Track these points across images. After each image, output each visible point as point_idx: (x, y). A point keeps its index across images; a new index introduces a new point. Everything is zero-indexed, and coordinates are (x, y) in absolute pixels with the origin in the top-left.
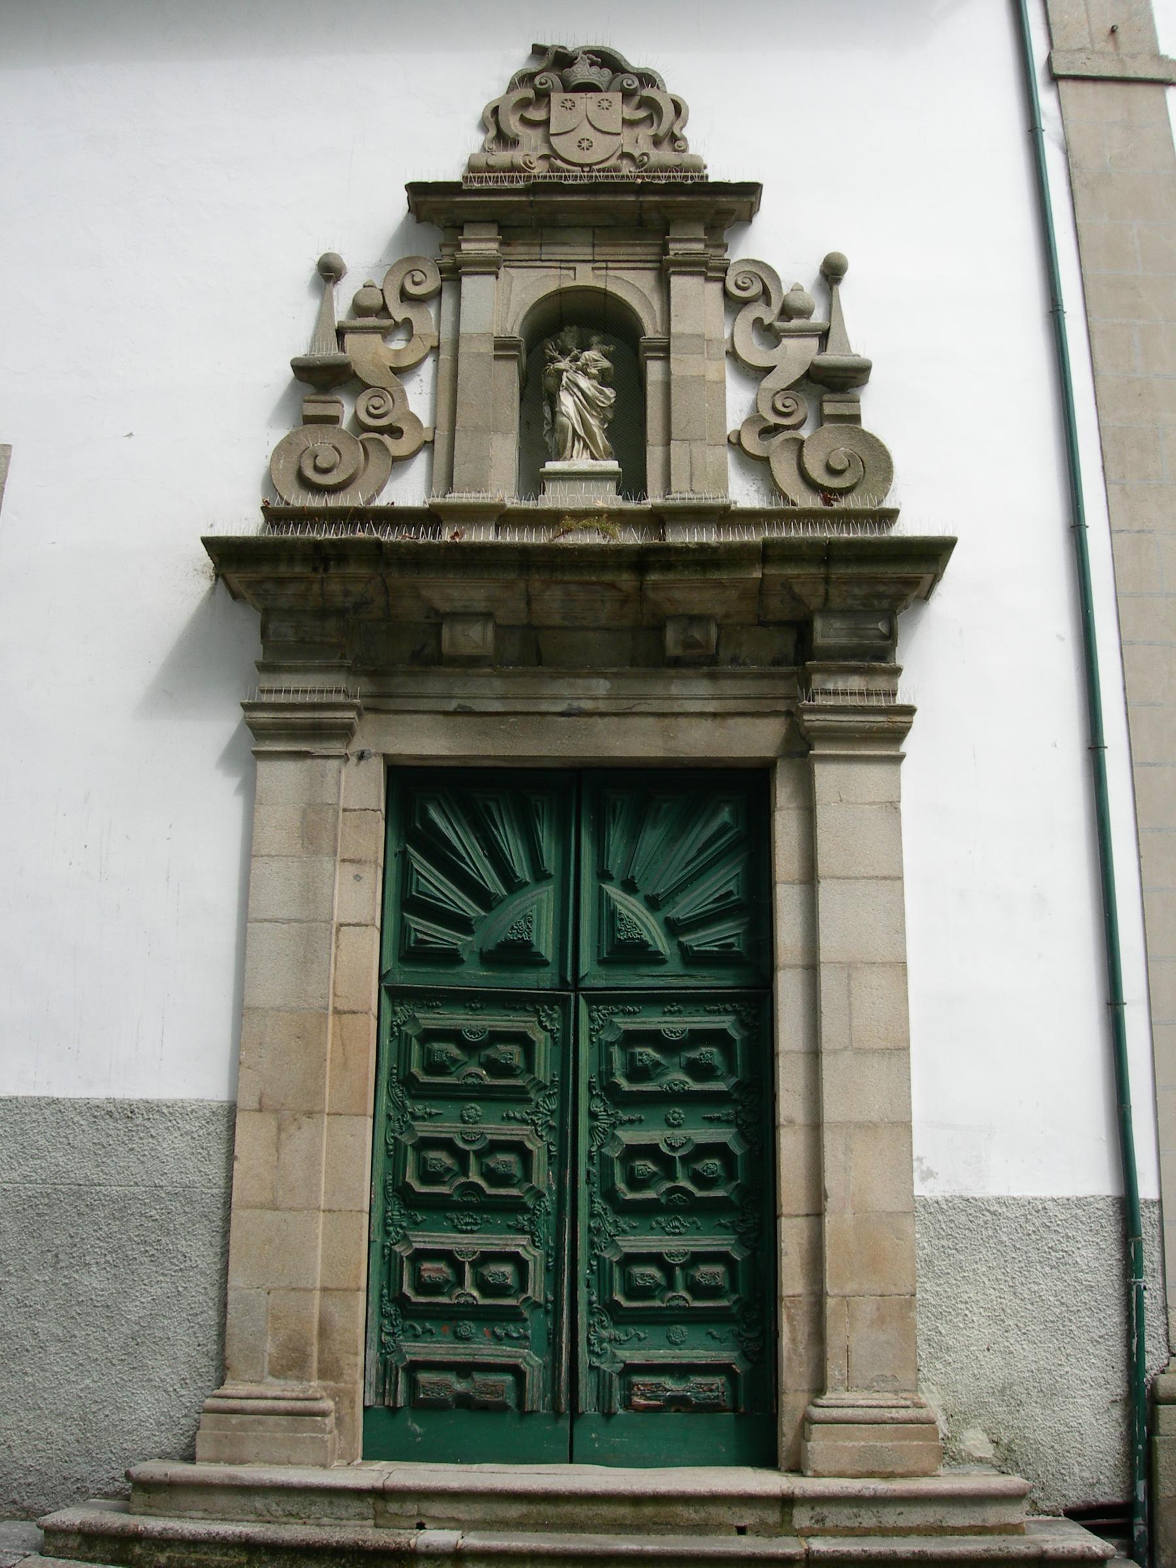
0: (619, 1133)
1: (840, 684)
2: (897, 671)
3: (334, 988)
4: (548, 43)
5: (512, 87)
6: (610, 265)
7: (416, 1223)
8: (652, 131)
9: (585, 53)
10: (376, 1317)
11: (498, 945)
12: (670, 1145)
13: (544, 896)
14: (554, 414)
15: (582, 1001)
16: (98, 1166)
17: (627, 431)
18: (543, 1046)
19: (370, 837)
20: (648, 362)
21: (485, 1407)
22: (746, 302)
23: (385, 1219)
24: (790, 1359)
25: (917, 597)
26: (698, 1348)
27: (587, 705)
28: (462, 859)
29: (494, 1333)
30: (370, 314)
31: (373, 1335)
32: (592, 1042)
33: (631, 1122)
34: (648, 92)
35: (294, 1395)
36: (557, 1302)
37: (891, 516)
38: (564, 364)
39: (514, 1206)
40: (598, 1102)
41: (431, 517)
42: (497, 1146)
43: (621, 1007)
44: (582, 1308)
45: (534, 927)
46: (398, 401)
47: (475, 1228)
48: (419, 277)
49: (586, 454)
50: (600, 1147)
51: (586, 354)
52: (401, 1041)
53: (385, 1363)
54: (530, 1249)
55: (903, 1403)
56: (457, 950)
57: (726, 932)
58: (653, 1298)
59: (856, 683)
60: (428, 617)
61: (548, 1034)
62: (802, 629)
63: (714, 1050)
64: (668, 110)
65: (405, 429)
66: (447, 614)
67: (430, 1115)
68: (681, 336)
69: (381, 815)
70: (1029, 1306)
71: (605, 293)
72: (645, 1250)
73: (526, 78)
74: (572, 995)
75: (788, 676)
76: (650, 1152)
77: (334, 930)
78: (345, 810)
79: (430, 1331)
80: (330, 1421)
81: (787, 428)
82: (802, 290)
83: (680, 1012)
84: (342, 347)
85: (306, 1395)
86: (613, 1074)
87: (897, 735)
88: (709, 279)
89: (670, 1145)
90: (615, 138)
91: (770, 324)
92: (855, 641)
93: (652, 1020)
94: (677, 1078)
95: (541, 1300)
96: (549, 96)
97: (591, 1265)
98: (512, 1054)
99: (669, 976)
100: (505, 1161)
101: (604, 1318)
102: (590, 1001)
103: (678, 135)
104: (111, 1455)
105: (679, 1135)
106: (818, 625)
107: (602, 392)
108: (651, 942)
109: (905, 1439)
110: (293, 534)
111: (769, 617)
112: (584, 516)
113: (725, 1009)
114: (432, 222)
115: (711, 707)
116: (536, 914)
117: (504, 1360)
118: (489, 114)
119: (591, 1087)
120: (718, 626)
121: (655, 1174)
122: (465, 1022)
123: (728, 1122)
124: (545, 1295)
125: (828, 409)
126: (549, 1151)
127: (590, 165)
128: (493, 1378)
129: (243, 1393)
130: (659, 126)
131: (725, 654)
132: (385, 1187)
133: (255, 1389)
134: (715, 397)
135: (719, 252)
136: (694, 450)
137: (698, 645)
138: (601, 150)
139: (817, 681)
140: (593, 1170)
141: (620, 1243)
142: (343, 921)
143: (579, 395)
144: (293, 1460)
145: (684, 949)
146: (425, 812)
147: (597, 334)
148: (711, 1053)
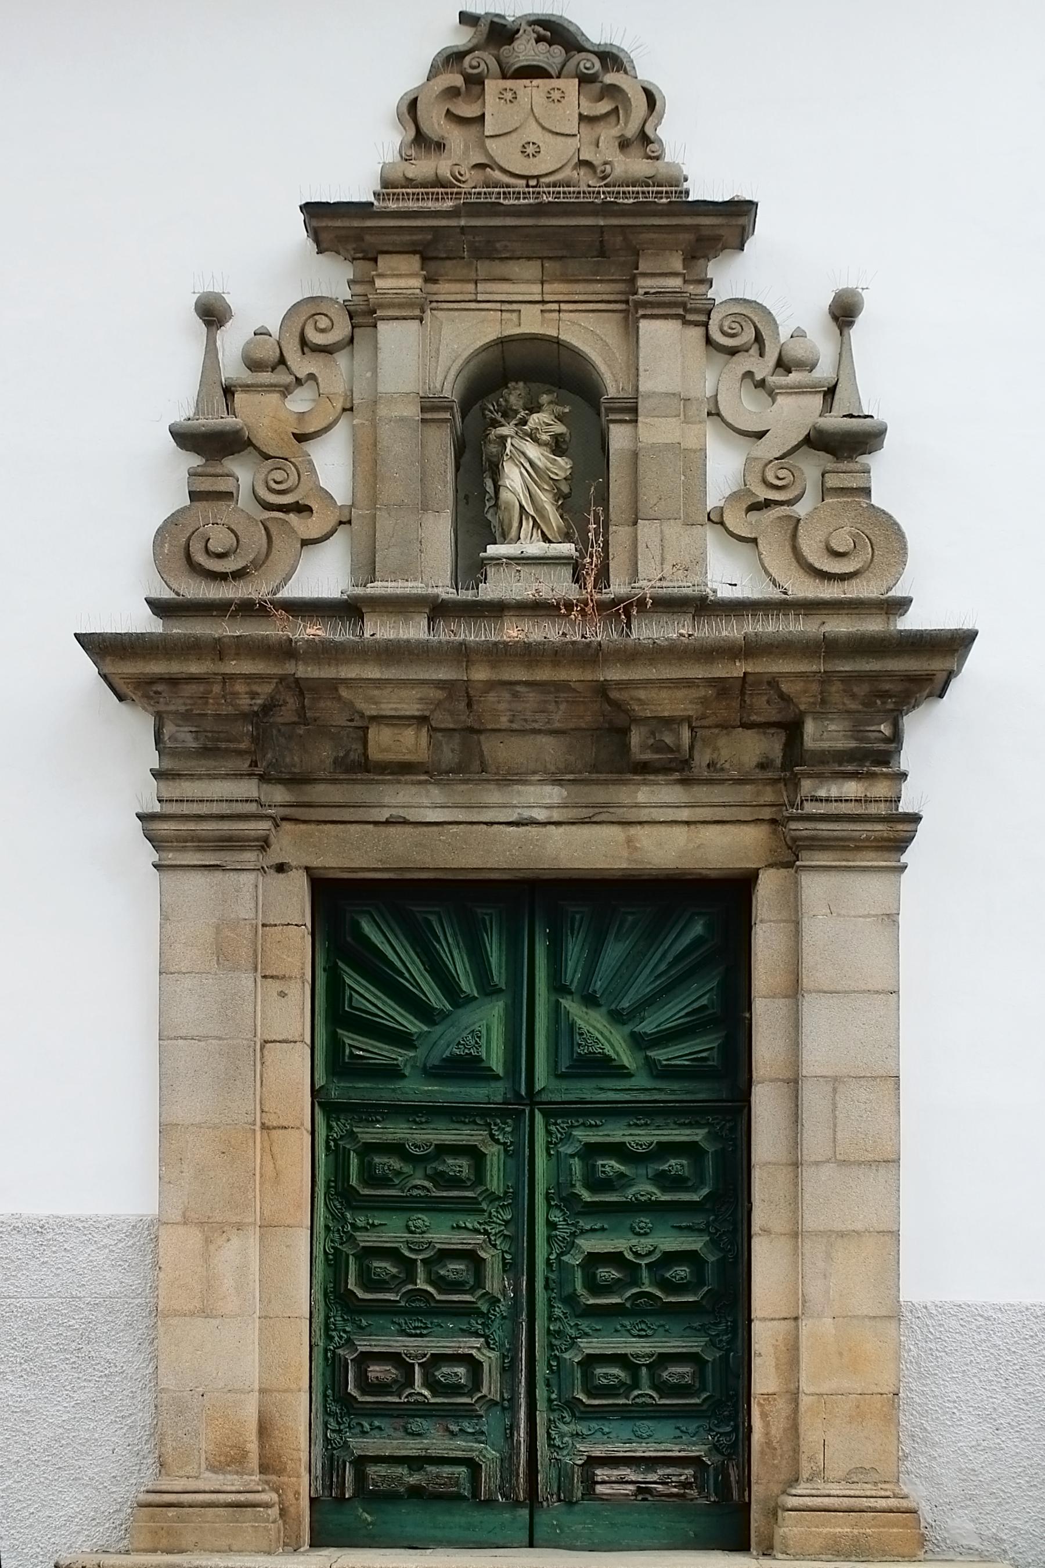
1: (834, 790)
3: (261, 1103)
4: (480, 11)
5: (434, 72)
6: (564, 306)
8: (615, 132)
9: (531, 23)
13: (495, 1012)
14: (497, 489)
15: (539, 1118)
16: (6, 1280)
17: (586, 498)
18: (495, 1158)
19: (296, 950)
20: (611, 426)
21: (439, 1497)
22: (733, 352)
26: (661, 1441)
27: (541, 815)
29: (447, 1430)
30: (267, 364)
31: (318, 1431)
32: (549, 1154)
33: (593, 1230)
34: (610, 78)
35: (234, 1488)
36: (513, 1400)
37: (902, 605)
39: (466, 1311)
40: (558, 1213)
41: (349, 610)
42: (446, 1255)
43: (581, 1121)
44: (541, 1405)
47: (425, 1332)
48: (323, 322)
49: (538, 535)
50: (559, 1255)
51: (535, 416)
52: (337, 1155)
54: (485, 1351)
55: (883, 1493)
56: (398, 1065)
58: (617, 1396)
59: (852, 788)
60: (352, 720)
61: (502, 1147)
62: (793, 729)
63: (684, 1162)
64: (639, 102)
65: (315, 507)
67: (373, 1225)
68: (651, 395)
69: (306, 931)
70: (1023, 1406)
71: (557, 342)
73: (452, 59)
75: (774, 782)
76: (615, 1259)
77: (258, 1047)
78: (263, 925)
79: (379, 1428)
80: (274, 1512)
81: (781, 503)
83: (646, 1124)
84: (230, 410)
85: (247, 1488)
86: (573, 1186)
87: (901, 844)
88: (686, 323)
90: (570, 140)
91: (763, 381)
92: (853, 744)
93: (617, 1133)
94: (645, 1189)
95: (498, 1398)
96: (483, 83)
98: (461, 1166)
99: (639, 1086)
101: (565, 1414)
102: (546, 1114)
103: (652, 137)
104: (38, 1550)
105: (644, 1244)
106: (810, 728)
108: (614, 1056)
109: (884, 1527)
110: (180, 629)
113: (697, 1122)
114: (338, 253)
115: (684, 814)
116: (486, 1028)
117: (459, 1454)
118: (404, 109)
119: (548, 1198)
120: (692, 729)
122: (408, 1136)
123: (700, 1231)
124: (502, 1393)
125: (832, 481)
127: (538, 177)
128: (446, 1470)
130: (626, 124)
133: (192, 1485)
134: (701, 447)
135: (701, 289)
136: (667, 532)
137: (669, 749)
138: (553, 157)
140: (553, 1276)
141: (582, 1345)
144: (235, 1548)
145: (651, 1065)
147: (549, 392)
148: (682, 1166)
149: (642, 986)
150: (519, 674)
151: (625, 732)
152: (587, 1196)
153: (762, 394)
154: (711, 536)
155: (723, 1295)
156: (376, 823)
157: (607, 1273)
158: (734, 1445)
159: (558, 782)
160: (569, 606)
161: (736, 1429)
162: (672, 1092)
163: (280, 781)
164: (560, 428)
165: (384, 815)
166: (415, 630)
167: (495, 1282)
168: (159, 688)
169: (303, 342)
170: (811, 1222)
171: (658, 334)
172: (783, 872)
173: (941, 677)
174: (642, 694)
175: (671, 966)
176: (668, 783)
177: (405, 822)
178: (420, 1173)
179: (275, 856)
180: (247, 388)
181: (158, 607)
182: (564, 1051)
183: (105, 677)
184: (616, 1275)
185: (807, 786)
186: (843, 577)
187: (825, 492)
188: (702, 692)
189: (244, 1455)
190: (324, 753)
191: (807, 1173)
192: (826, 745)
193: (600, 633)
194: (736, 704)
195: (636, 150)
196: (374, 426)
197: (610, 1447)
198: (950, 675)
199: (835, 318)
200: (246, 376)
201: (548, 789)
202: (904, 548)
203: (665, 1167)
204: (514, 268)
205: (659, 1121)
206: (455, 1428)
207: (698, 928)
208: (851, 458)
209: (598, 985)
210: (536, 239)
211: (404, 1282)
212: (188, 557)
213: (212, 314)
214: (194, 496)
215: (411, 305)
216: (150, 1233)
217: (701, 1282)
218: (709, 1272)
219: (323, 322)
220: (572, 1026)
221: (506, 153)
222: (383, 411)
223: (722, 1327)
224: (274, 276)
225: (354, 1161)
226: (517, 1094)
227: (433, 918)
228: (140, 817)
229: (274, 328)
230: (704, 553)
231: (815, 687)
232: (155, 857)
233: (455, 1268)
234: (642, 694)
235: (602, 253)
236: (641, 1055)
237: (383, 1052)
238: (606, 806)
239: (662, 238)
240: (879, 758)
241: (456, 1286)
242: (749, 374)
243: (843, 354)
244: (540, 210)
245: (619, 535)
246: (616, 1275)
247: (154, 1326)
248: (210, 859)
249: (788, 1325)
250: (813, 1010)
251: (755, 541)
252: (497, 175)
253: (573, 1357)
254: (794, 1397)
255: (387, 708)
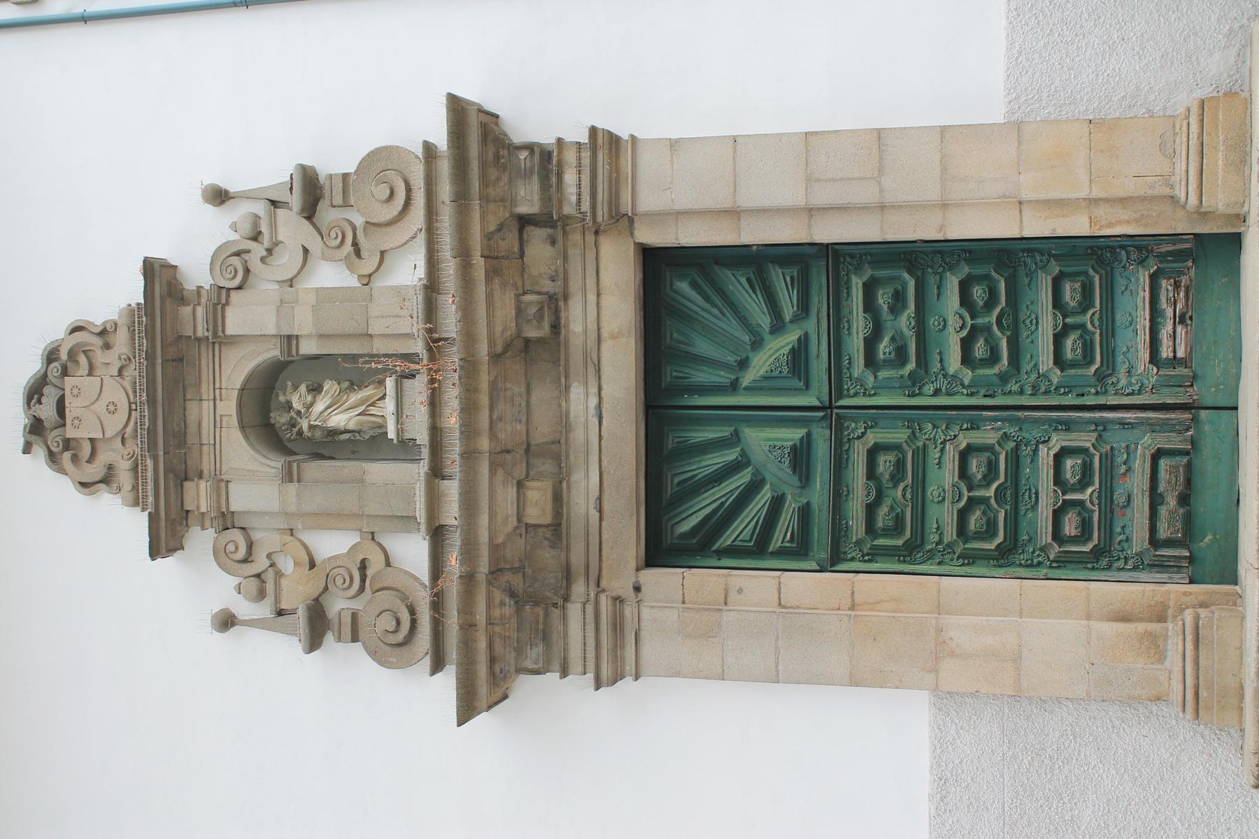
0: (951, 371)
2: (560, 141)
5: (62, 471)
6: (217, 386)
7: (1030, 540)
8: (99, 352)
10: (1111, 574)
11: (794, 471)
12: (961, 328)
17: (354, 370)
19: (703, 581)
21: (1189, 482)
22: (247, 271)
23: (1027, 566)
24: (1146, 226)
25: (497, 124)
27: (593, 401)
28: (723, 504)
29: (1124, 474)
30: (260, 586)
31: (1125, 575)
33: (941, 361)
34: (64, 356)
35: (1180, 643)
37: (429, 149)
38: (305, 426)
41: (437, 534)
42: (963, 473)
44: (1101, 400)
45: (779, 444)
46: (339, 563)
47: (1033, 491)
48: (231, 547)
49: (380, 404)
52: (875, 554)
53: (1152, 566)
54: (1051, 444)
55: (1185, 128)
57: (819, 281)
59: (570, 177)
63: (881, 292)
64: (79, 337)
65: (362, 557)
66: (519, 520)
67: (938, 529)
68: (278, 325)
69: (687, 572)
72: (1051, 348)
73: (53, 458)
74: (836, 411)
75: (565, 233)
76: (967, 344)
79: (1123, 527)
82: (234, 224)
84: (293, 612)
87: (614, 141)
89: (961, 328)
94: (905, 322)
95: (1095, 434)
97: (1064, 393)
98: (885, 463)
99: (816, 327)
100: (976, 467)
105: (953, 322)
106: (523, 209)
107: (327, 393)
108: (790, 346)
111: (516, 249)
112: (434, 403)
115: (592, 298)
116: (766, 443)
118: (86, 490)
120: (525, 293)
121: (986, 340)
125: (338, 200)
126: (967, 429)
127: (130, 403)
128: (1163, 475)
129: (1181, 687)
131: (548, 286)
132: (1000, 566)
135: (204, 293)
138: (116, 393)
139: (568, 210)
140: (983, 392)
142: (776, 604)
143: (334, 411)
145: (796, 319)
146: (684, 536)
147: (277, 396)
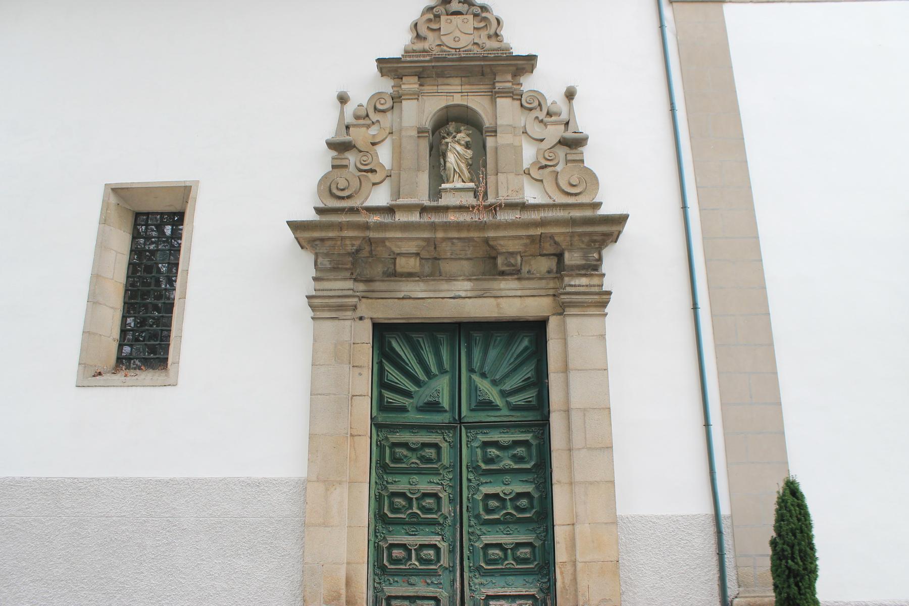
5: (423, 14)
8: (486, 33)
14: (445, 162)
17: (478, 165)
19: (366, 354)
22: (531, 109)
27: (463, 294)
30: (362, 117)
31: (371, 583)
34: (484, 15)
37: (598, 205)
39: (434, 523)
41: (390, 210)
42: (426, 495)
44: (466, 569)
48: (383, 101)
49: (460, 180)
50: (473, 495)
52: (381, 448)
58: (498, 564)
59: (584, 281)
62: (560, 256)
64: (495, 23)
68: (502, 126)
71: (467, 107)
73: (430, 9)
76: (496, 496)
84: (348, 134)
87: (604, 304)
88: (514, 99)
92: (584, 262)
93: (495, 436)
94: (508, 463)
98: (431, 453)
99: (504, 414)
102: (466, 428)
105: (508, 489)
106: (567, 255)
115: (519, 293)
116: (441, 388)
117: (431, 595)
119: (467, 468)
125: (570, 157)
134: (519, 145)
135: (518, 87)
137: (513, 266)
138: (465, 42)
140: (470, 505)
149: (504, 369)
150: (454, 234)
151: (495, 258)
152: (484, 466)
153: (542, 125)
154: (526, 180)
155: (541, 514)
156: (399, 298)
157: (493, 503)
158: (549, 588)
159: (470, 280)
160: (473, 207)
161: (549, 580)
162: (518, 416)
163: (361, 281)
164: (468, 139)
165: (401, 295)
166: (415, 217)
167: (446, 508)
168: (317, 243)
169: (375, 109)
170: (578, 477)
171: (504, 103)
172: (559, 317)
173: (616, 233)
174: (502, 242)
175: (516, 359)
176: (512, 280)
177: (410, 298)
178: (415, 456)
179: (359, 313)
180: (355, 126)
181: (319, 211)
182: (473, 398)
183: (297, 239)
184: (497, 504)
185: (567, 280)
186: (576, 195)
187: (567, 161)
188: (525, 241)
189: (339, 595)
190: (379, 269)
191: (575, 453)
192: (573, 263)
193: (486, 218)
194: (538, 246)
195: (494, 39)
196: (400, 139)
197: (496, 590)
198: (620, 233)
199: (567, 97)
200: (354, 121)
201: (466, 283)
202: (598, 183)
203: (515, 452)
204: (451, 81)
205: (513, 430)
206: (429, 581)
207: (526, 343)
208: (576, 149)
209: (486, 369)
210: (460, 75)
211: (408, 509)
212: (330, 191)
213: (343, 99)
214: (334, 167)
215: (414, 94)
216: (303, 485)
217: (532, 507)
218: (536, 502)
219: (383, 101)
220: (476, 387)
221: (448, 41)
222: (404, 133)
223: (542, 529)
224: (365, 83)
225: (388, 451)
226: (454, 418)
227: (420, 340)
228: (308, 297)
229: (365, 104)
230: (523, 186)
231: (568, 239)
232: (312, 314)
233: (429, 502)
234: (502, 242)
235: (483, 75)
236: (504, 400)
237: (399, 400)
238: (489, 289)
239: (505, 69)
240: (593, 268)
241: (428, 510)
242: (537, 118)
243: (571, 110)
244: (461, 59)
245: (491, 179)
246: (497, 504)
247: (303, 531)
248: (334, 315)
249: (570, 527)
250: (574, 377)
251: (541, 181)
252: (445, 48)
253: (479, 545)
254: (574, 563)
255: (404, 250)
